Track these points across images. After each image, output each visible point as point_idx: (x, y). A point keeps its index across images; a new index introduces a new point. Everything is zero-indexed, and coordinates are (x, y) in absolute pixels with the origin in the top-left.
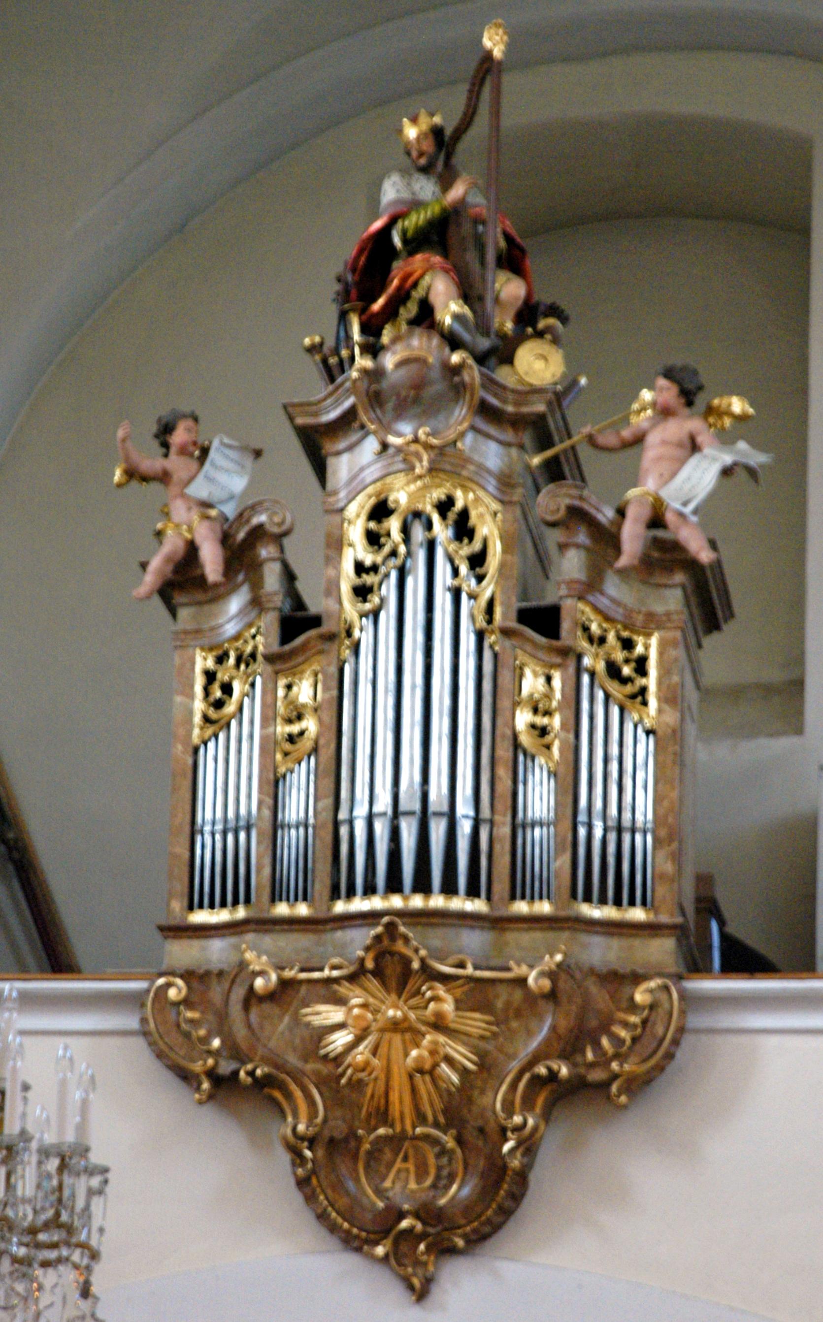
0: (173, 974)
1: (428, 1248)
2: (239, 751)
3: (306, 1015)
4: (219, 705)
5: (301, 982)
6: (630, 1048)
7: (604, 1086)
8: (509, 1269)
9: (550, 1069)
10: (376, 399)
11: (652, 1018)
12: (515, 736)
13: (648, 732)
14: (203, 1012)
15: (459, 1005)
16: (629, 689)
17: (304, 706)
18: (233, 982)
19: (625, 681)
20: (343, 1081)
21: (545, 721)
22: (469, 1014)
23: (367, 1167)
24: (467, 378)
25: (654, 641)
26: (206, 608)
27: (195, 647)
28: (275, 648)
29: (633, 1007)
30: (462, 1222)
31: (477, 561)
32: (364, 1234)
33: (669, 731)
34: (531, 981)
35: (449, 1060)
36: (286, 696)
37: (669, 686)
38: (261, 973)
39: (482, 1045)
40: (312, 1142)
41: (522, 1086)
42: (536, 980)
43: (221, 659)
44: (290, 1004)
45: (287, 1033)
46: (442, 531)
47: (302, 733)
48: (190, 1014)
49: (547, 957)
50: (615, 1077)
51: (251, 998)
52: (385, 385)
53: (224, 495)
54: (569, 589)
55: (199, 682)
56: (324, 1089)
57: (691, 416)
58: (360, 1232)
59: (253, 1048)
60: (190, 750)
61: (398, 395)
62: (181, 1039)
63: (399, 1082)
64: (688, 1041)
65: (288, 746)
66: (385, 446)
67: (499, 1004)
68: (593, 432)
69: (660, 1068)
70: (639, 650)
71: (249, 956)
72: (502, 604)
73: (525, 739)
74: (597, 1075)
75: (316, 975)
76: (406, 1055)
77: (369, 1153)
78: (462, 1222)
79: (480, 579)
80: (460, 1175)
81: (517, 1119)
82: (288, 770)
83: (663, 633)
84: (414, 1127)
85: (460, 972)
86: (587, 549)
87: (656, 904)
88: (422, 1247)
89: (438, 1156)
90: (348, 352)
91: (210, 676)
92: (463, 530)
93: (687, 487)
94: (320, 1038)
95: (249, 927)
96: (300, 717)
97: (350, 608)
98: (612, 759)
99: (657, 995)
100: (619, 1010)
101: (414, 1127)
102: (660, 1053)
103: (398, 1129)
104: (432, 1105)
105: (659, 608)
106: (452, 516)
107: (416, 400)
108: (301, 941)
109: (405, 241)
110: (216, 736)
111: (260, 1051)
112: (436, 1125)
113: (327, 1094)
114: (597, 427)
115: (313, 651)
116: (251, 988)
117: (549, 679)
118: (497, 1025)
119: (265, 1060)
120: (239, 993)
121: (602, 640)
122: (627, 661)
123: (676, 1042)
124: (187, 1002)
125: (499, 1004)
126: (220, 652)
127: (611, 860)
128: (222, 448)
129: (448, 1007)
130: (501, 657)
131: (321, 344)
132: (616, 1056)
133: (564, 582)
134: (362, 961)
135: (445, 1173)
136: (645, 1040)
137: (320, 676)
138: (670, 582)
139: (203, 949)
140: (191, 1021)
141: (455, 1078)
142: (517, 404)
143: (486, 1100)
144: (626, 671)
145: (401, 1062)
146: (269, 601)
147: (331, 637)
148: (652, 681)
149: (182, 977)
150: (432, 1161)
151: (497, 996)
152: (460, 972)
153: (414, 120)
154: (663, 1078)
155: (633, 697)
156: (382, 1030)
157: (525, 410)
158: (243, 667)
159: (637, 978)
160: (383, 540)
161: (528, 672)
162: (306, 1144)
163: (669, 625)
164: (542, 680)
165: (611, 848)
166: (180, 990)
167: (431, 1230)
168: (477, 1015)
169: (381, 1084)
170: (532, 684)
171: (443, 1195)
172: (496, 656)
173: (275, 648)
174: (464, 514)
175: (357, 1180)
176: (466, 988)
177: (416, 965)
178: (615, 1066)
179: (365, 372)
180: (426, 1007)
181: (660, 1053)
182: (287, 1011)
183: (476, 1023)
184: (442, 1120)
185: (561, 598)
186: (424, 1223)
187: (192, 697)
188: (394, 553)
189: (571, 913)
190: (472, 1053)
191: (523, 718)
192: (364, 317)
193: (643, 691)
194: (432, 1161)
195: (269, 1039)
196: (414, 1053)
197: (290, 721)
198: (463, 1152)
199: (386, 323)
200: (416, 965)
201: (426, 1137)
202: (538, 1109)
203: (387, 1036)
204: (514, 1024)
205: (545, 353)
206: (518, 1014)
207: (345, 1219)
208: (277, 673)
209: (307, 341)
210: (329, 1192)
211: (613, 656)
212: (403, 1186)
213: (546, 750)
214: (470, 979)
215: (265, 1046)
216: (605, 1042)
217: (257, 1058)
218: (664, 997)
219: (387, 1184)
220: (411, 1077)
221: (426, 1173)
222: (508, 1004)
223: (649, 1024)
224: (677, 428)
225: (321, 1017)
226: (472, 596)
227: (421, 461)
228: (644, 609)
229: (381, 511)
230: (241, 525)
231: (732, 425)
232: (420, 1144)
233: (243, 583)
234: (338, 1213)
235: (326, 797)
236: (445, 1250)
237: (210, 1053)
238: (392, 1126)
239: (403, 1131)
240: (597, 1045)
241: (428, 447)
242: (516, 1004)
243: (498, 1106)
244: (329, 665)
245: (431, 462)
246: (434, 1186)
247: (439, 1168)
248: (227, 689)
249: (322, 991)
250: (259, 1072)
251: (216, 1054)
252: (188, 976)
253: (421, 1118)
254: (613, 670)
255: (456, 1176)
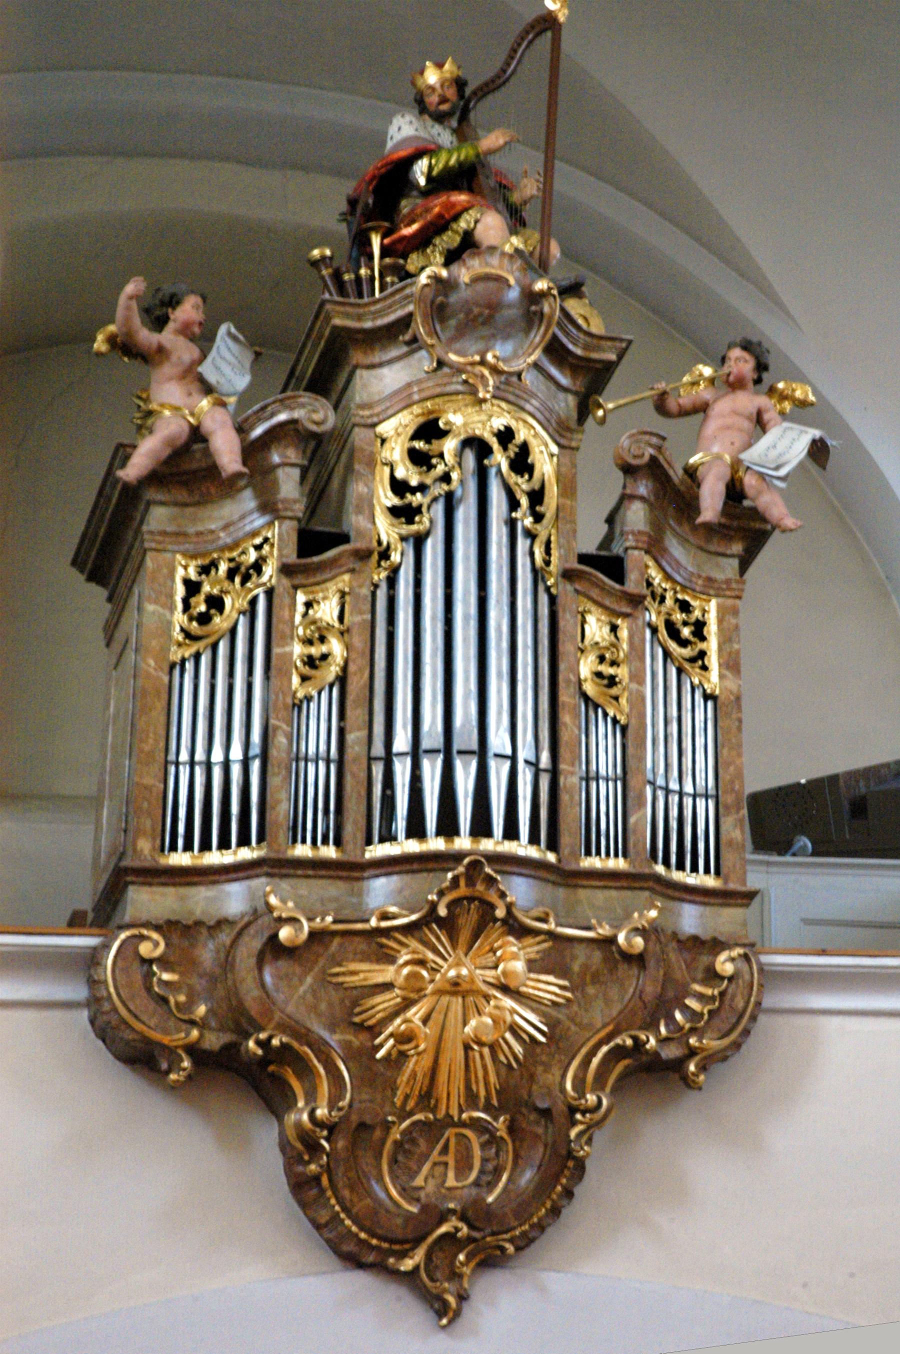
0: (146, 925)
1: (469, 1258)
2: (231, 674)
3: (337, 974)
4: (204, 619)
5: (334, 933)
6: (707, 1022)
7: (678, 1065)
8: (556, 1281)
9: (635, 1039)
10: (439, 312)
11: (730, 991)
12: (580, 683)
13: (707, 697)
14: (181, 974)
15: (532, 966)
16: (687, 652)
17: (329, 627)
18: (240, 934)
19: (684, 643)
20: (379, 1055)
21: (611, 671)
22: (544, 977)
23: (394, 1161)
24: (546, 309)
25: (713, 606)
26: (189, 510)
27: (175, 552)
28: (292, 557)
29: (712, 976)
30: (514, 1223)
31: (537, 497)
32: (385, 1245)
33: (732, 698)
34: (621, 938)
35: (514, 1029)
36: (305, 615)
37: (730, 653)
38: (292, 920)
39: (553, 1012)
40: (332, 1129)
41: (595, 1061)
42: (627, 939)
43: (205, 570)
44: (315, 962)
45: (309, 997)
46: (500, 459)
47: (324, 657)
48: (166, 976)
49: (636, 915)
50: (692, 1052)
51: (274, 948)
52: (453, 299)
53: (232, 390)
54: (637, 541)
55: (180, 591)
56: (351, 1064)
57: (757, 393)
58: (364, 1247)
59: (268, 1012)
60: (166, 668)
61: (469, 312)
62: (152, 1006)
63: (454, 1055)
64: (762, 1018)
65: (306, 670)
66: (441, 364)
67: (576, 968)
68: (668, 390)
69: (737, 1046)
70: (697, 614)
71: (273, 900)
72: (560, 547)
73: (590, 688)
74: (671, 1052)
75: (359, 926)
76: (465, 1023)
77: (398, 1145)
78: (514, 1223)
79: (538, 518)
80: (509, 1166)
81: (591, 1098)
82: (306, 697)
83: (721, 600)
84: (461, 1111)
85: (544, 926)
86: (651, 506)
87: (724, 870)
88: (461, 1257)
89: (483, 1146)
90: (369, 272)
91: (192, 588)
92: (522, 463)
93: (773, 454)
94: (355, 1003)
95: (258, 871)
96: (322, 639)
97: (386, 529)
98: (672, 721)
99: (739, 965)
100: (694, 980)
101: (461, 1111)
102: (740, 1028)
103: (441, 1114)
104: (487, 1084)
105: (719, 576)
106: (513, 450)
107: (488, 321)
108: (332, 889)
109: (429, 178)
110: (197, 656)
111: (277, 1015)
112: (488, 1108)
113: (353, 1070)
114: (671, 386)
115: (344, 569)
116: (275, 936)
117: (614, 629)
118: (573, 992)
119: (283, 1028)
120: (253, 943)
121: (663, 599)
122: (685, 624)
123: (753, 1018)
124: (164, 962)
125: (576, 968)
126: (207, 561)
127: (674, 825)
128: (227, 339)
129: (519, 966)
130: (561, 601)
131: (331, 258)
132: (693, 1030)
133: (633, 533)
134: (434, 906)
135: (490, 1167)
136: (723, 1014)
137: (347, 598)
138: (729, 552)
139: (182, 899)
140: (167, 983)
141: (518, 1049)
142: (586, 347)
143: (552, 1078)
144: (686, 632)
145: (459, 1030)
146: (286, 509)
147: (363, 555)
148: (712, 645)
149: (158, 928)
150: (477, 1152)
151: (574, 958)
152: (544, 926)
153: (440, 65)
154: (736, 1060)
155: (692, 660)
156: (439, 992)
157: (595, 355)
158: (237, 580)
159: (717, 945)
160: (434, 461)
161: (590, 618)
162: (325, 1133)
163: (728, 593)
164: (606, 629)
165: (674, 813)
166: (156, 944)
167: (476, 1235)
168: (551, 978)
169: (426, 1062)
170: (596, 628)
171: (490, 1191)
172: (553, 600)
173: (292, 557)
174: (524, 449)
175: (380, 1179)
176: (545, 945)
177: (500, 913)
178: (693, 1041)
179: (437, 279)
180: (496, 967)
181: (740, 1028)
182: (311, 970)
183: (548, 988)
184: (495, 1102)
185: (626, 549)
186: (471, 1226)
187: (172, 609)
188: (446, 478)
189: (647, 871)
190: (542, 1022)
191: (587, 667)
192: (386, 241)
193: (702, 654)
194: (477, 1152)
195: (287, 1002)
196: (473, 1023)
197: (309, 642)
198: (514, 1142)
199: (412, 251)
200: (500, 913)
201: (475, 1124)
202: (608, 1089)
203: (445, 999)
204: (591, 990)
205: (588, 315)
206: (596, 978)
207: (362, 1229)
208: (296, 588)
209: (316, 253)
210: (346, 1193)
211: (673, 618)
212: (442, 1179)
213: (614, 702)
214: (551, 934)
215: (282, 1012)
216: (678, 1016)
217: (272, 1026)
218: (745, 968)
219: (419, 1181)
220: (467, 1048)
221: (471, 1168)
222: (585, 967)
223: (728, 997)
224: (747, 401)
225: (362, 976)
226: (531, 535)
227: (486, 385)
228: (704, 575)
229: (430, 430)
230: (261, 420)
231: (791, 410)
232: (468, 1132)
233: (246, 487)
234: (355, 1222)
235: (359, 729)
236: (490, 1260)
237: (193, 1023)
238: (434, 1111)
239: (448, 1115)
240: (670, 1019)
241: (495, 370)
242: (594, 968)
243: (569, 1086)
244: (360, 586)
245: (496, 388)
246: (477, 1184)
247: (485, 1160)
248: (215, 603)
249: (361, 945)
250: (275, 1042)
251: (202, 1025)
252: (167, 927)
253: (472, 1099)
254: (673, 631)
255: (505, 1168)
